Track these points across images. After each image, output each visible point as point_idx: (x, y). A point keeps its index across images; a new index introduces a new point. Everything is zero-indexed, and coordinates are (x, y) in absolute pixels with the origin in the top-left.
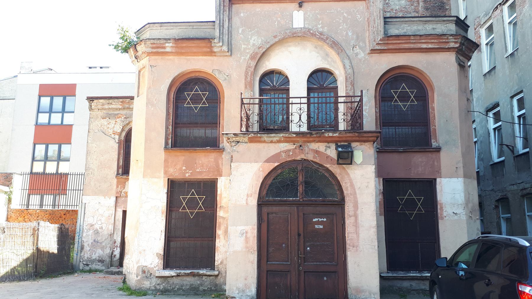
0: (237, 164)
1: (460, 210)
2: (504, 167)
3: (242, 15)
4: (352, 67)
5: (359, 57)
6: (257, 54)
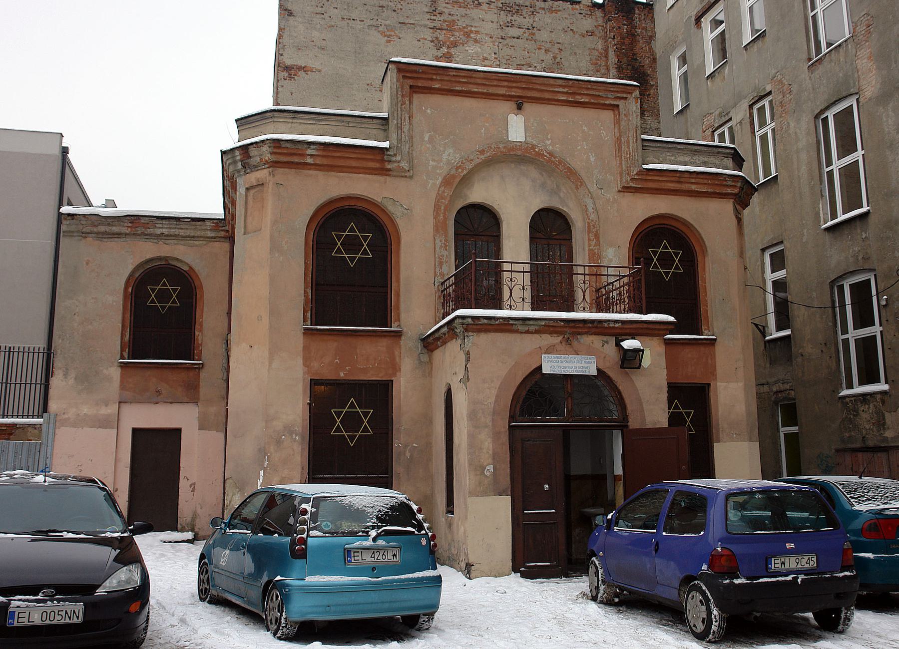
6: (454, 177)
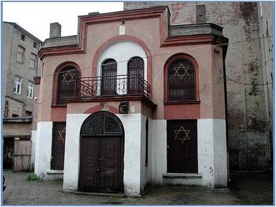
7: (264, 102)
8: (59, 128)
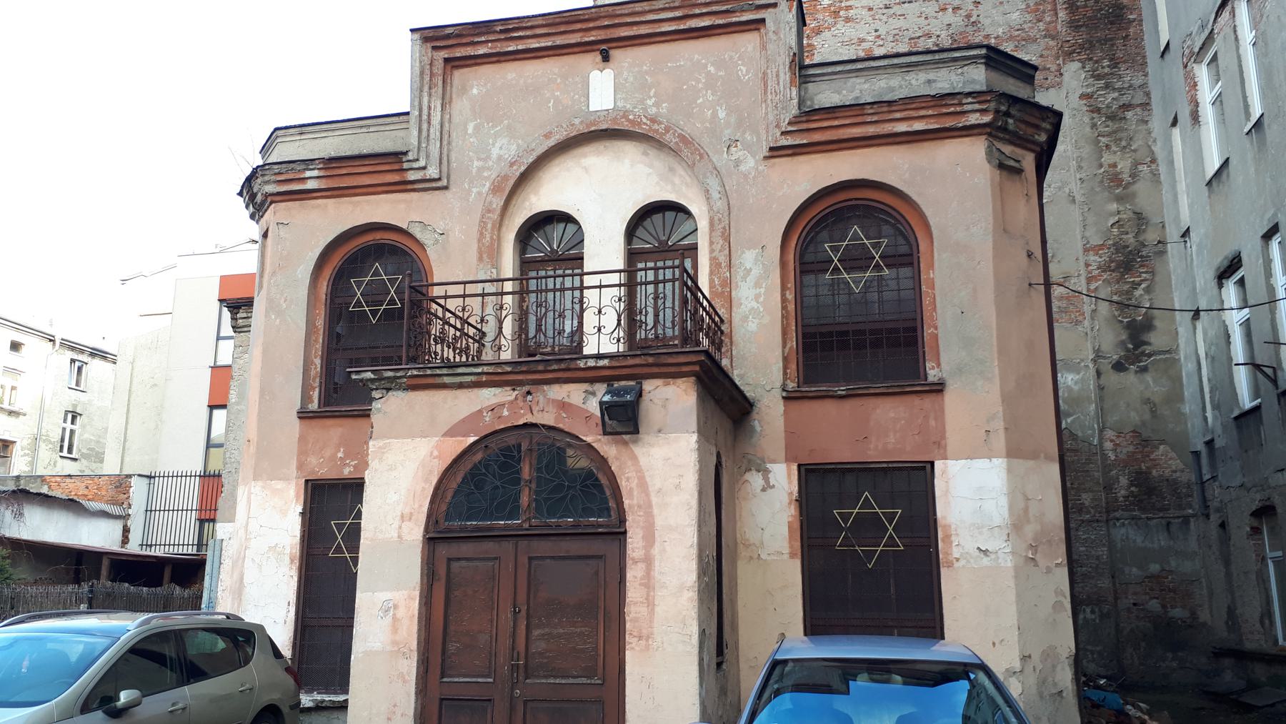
0: (381, 443)
1: (997, 543)
2: (1261, 423)
3: (475, 91)
4: (725, 194)
5: (743, 168)
6: (506, 178)
7: (1181, 399)
8: (331, 508)
